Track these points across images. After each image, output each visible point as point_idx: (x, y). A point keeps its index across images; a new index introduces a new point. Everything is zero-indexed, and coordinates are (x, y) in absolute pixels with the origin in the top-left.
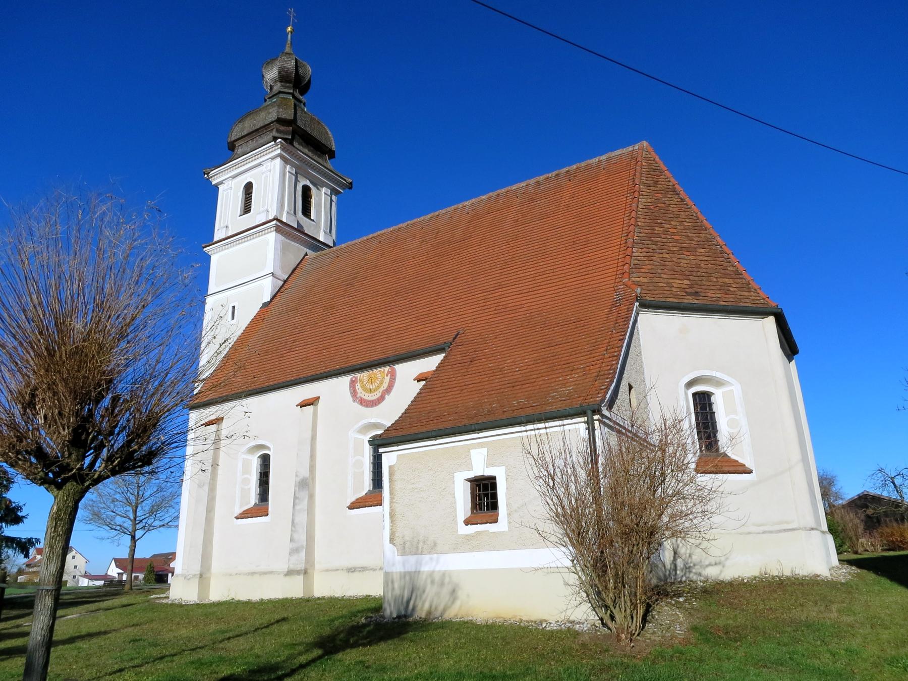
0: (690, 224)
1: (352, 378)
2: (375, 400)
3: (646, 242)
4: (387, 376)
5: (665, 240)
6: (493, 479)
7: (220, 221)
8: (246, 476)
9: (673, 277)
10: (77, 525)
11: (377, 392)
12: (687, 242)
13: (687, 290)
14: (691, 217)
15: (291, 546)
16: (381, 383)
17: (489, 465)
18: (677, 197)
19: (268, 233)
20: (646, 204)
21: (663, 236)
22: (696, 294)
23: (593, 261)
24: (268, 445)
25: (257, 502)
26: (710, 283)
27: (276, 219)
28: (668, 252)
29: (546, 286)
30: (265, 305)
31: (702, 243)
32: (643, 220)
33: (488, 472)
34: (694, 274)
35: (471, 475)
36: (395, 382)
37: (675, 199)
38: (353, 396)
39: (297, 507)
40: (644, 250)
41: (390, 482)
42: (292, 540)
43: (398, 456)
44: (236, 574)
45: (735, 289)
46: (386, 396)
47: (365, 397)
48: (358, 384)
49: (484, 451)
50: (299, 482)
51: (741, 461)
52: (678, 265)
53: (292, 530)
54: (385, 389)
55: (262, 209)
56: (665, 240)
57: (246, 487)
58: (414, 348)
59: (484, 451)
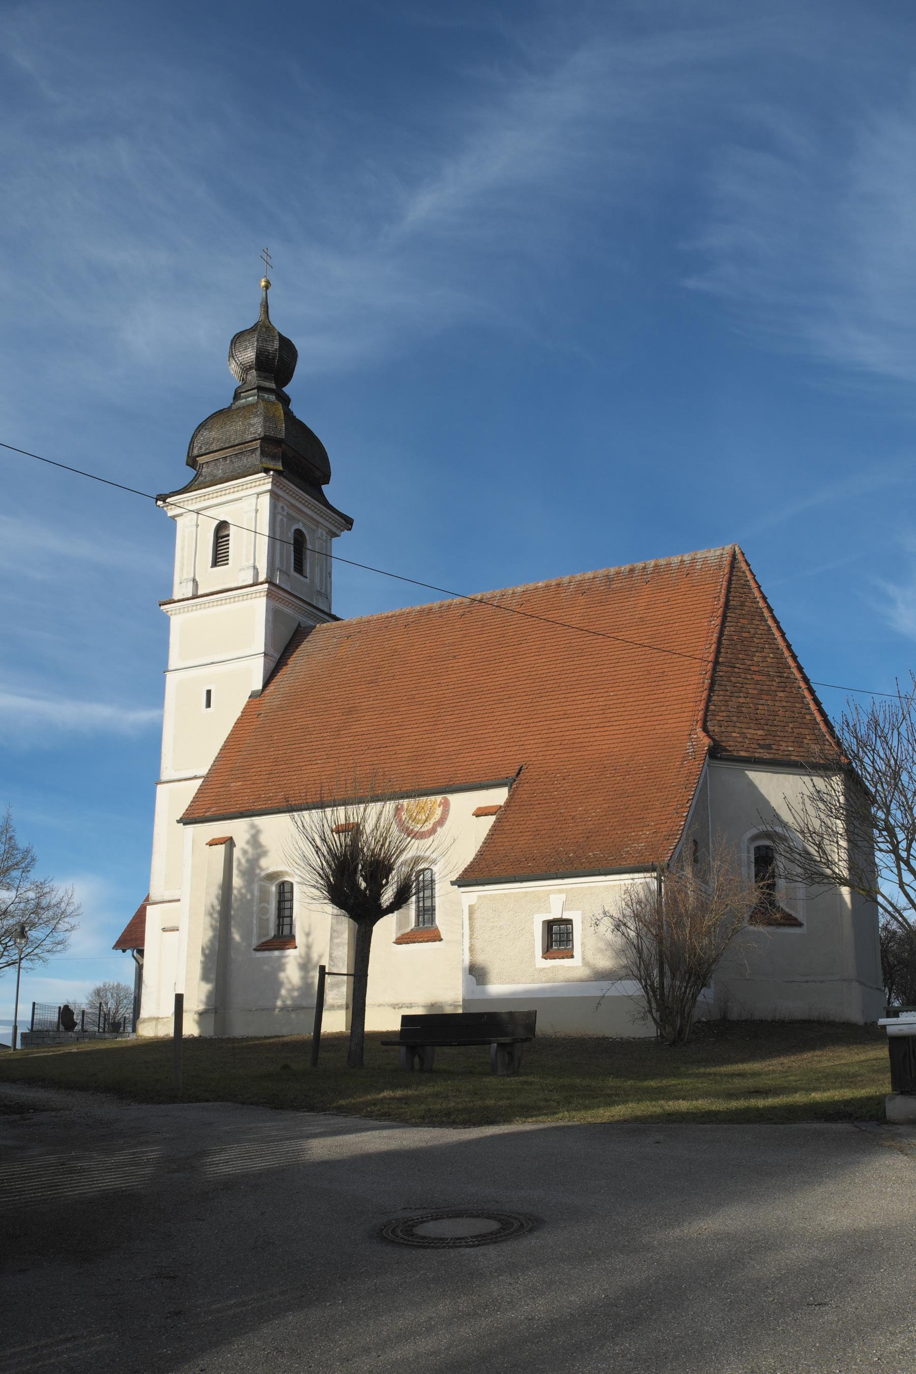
4: (439, 806)
6: (569, 922)
7: (182, 569)
13: (760, 742)
15: (75, 1012)
18: (764, 624)
19: (256, 598)
22: (768, 747)
25: (276, 933)
34: (770, 723)
35: (550, 917)
36: (448, 815)
43: (479, 897)
44: (256, 1010)
46: (439, 829)
49: (563, 897)
51: (794, 914)
57: (264, 917)
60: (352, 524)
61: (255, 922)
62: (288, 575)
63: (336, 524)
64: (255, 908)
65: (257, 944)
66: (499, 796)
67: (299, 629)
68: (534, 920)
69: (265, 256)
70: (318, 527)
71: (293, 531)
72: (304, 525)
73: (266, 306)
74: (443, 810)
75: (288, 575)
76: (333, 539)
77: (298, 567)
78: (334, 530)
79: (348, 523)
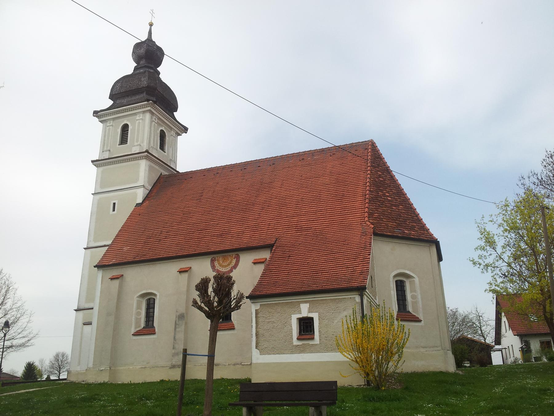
0: (395, 191)
1: (212, 258)
2: (226, 272)
3: (375, 200)
5: (383, 200)
8: (139, 310)
9: (388, 220)
10: (494, 317)
11: (228, 267)
12: (394, 201)
14: (396, 187)
16: (231, 262)
17: (309, 312)
20: (374, 178)
21: (383, 197)
23: (348, 207)
24: (152, 291)
25: (145, 326)
26: (406, 225)
27: (147, 151)
28: (385, 206)
29: (323, 218)
30: (138, 205)
31: (402, 202)
32: (373, 188)
33: (310, 315)
35: (300, 316)
37: (388, 176)
38: (212, 269)
39: (177, 330)
40: (374, 205)
41: (256, 318)
42: (173, 348)
45: (417, 229)
46: (234, 270)
47: (220, 270)
48: (216, 262)
50: (179, 316)
51: (417, 316)
52: (391, 214)
53: (174, 343)
54: (233, 266)
55: (136, 144)
56: (383, 200)
58: (251, 245)
59: (307, 305)
60: (187, 130)
61: (133, 320)
62: (157, 150)
63: (180, 130)
64: (134, 312)
65: (134, 332)
66: (266, 255)
67: (161, 176)
68: (292, 318)
69: (151, 12)
70: (171, 130)
71: (160, 130)
72: (165, 128)
73: (150, 33)
74: (236, 260)
75: (157, 150)
76: (178, 137)
77: (161, 145)
78: (179, 132)
79: (185, 130)
